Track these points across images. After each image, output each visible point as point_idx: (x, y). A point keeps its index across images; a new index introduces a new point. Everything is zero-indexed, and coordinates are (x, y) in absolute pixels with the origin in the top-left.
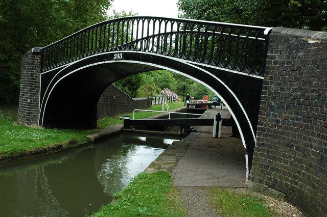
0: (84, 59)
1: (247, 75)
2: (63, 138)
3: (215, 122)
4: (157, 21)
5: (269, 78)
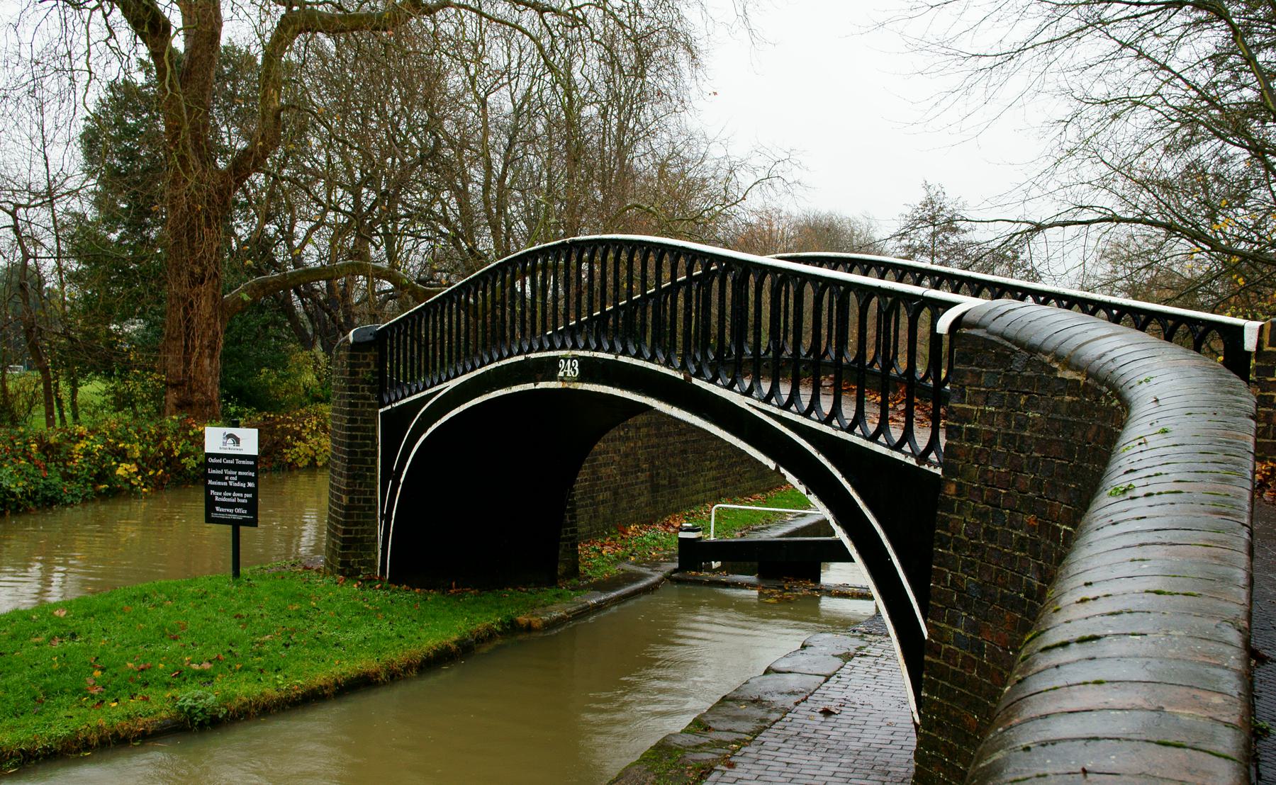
0: (404, 401)
2: (444, 626)
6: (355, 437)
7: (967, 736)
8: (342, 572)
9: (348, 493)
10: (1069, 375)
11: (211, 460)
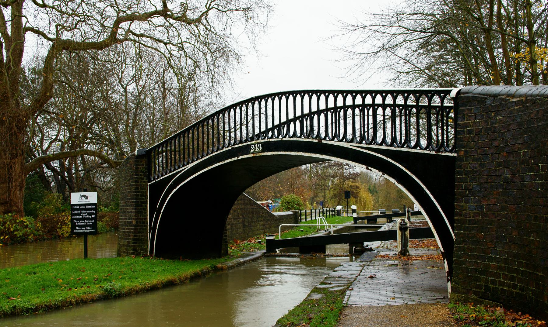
0: (163, 177)
1: (434, 153)
3: (399, 234)
4: (298, 96)
6: (138, 195)
7: (479, 242)
8: (133, 254)
9: (136, 219)
10: (515, 100)
11: (74, 207)
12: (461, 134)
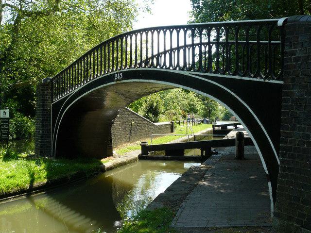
1: (262, 80)
5: (289, 80)
12: (288, 62)
